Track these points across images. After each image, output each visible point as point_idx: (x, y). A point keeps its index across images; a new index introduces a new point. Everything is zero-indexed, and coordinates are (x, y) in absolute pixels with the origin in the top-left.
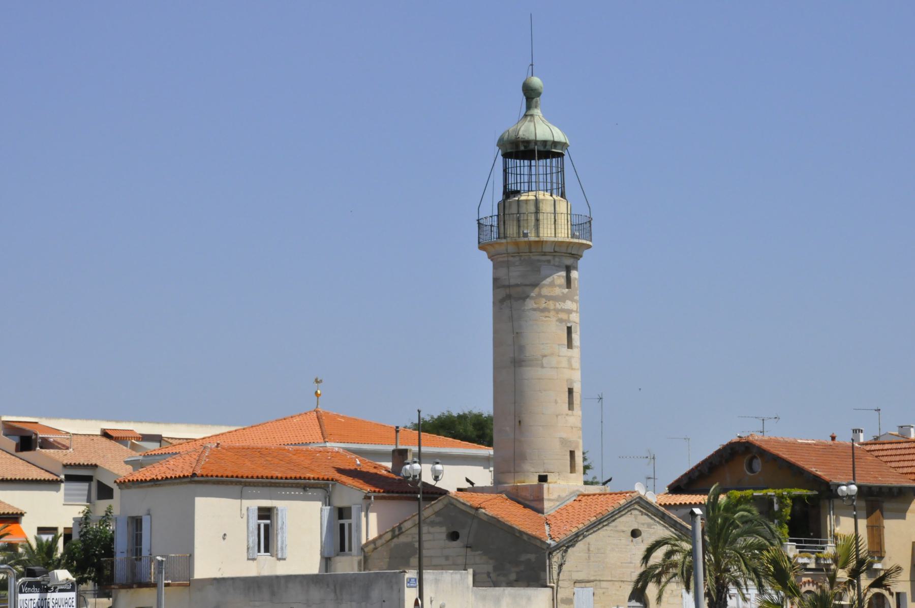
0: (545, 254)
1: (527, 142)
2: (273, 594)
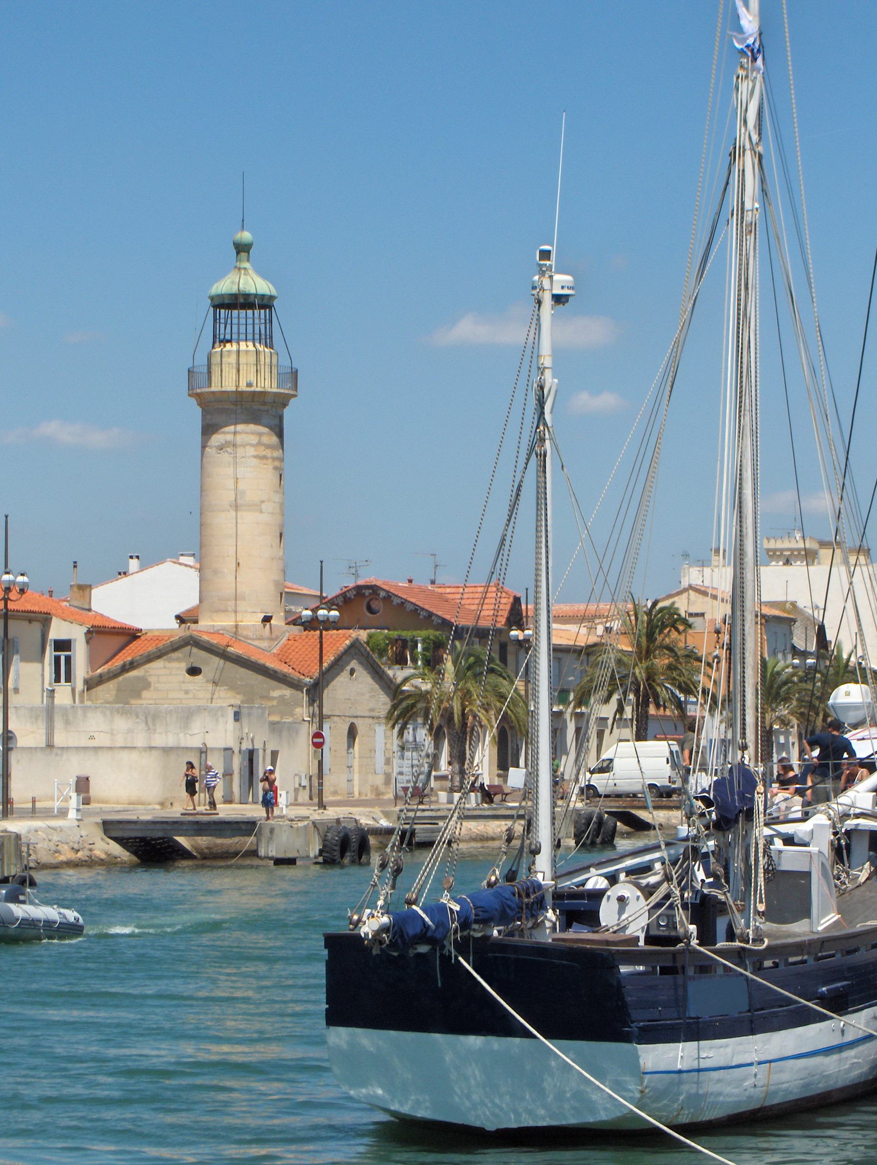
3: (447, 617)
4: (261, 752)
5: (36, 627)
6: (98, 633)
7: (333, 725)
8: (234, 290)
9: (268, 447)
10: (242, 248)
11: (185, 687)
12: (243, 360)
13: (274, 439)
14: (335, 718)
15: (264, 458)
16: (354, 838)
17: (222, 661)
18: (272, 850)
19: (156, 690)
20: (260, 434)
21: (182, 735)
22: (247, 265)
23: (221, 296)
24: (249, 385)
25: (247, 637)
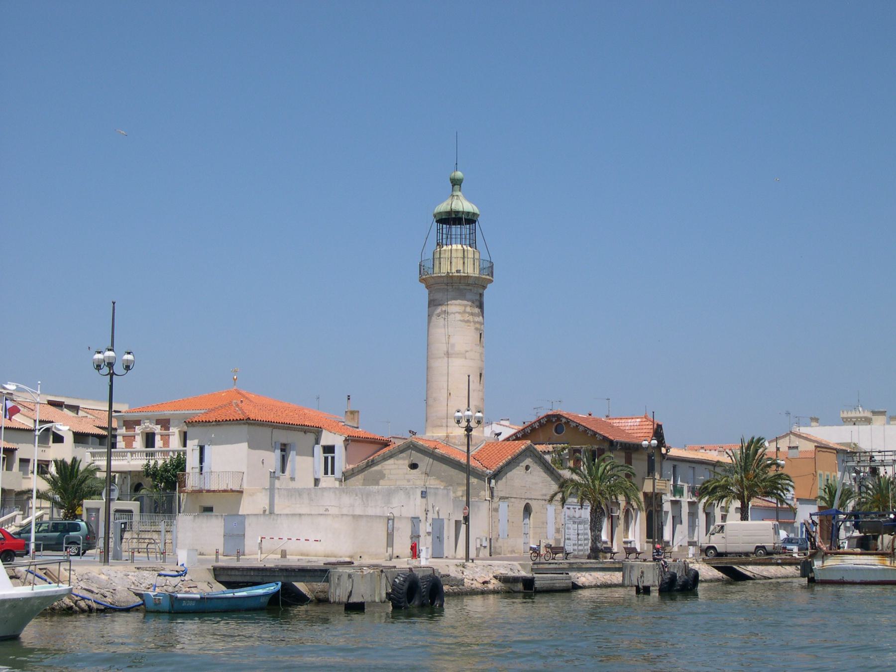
0: (469, 285)
1: (457, 212)
2: (311, 500)
3: (607, 435)
4: (446, 522)
5: (311, 437)
6: (353, 441)
7: (510, 504)
8: (448, 209)
9: (472, 314)
10: (456, 183)
11: (407, 477)
12: (454, 255)
13: (477, 310)
14: (513, 500)
15: (468, 321)
16: (424, 587)
17: (431, 460)
18: (339, 593)
19: (389, 479)
20: (466, 306)
21: (385, 508)
22: (459, 193)
23: (440, 213)
24: (458, 271)
25: (454, 444)
